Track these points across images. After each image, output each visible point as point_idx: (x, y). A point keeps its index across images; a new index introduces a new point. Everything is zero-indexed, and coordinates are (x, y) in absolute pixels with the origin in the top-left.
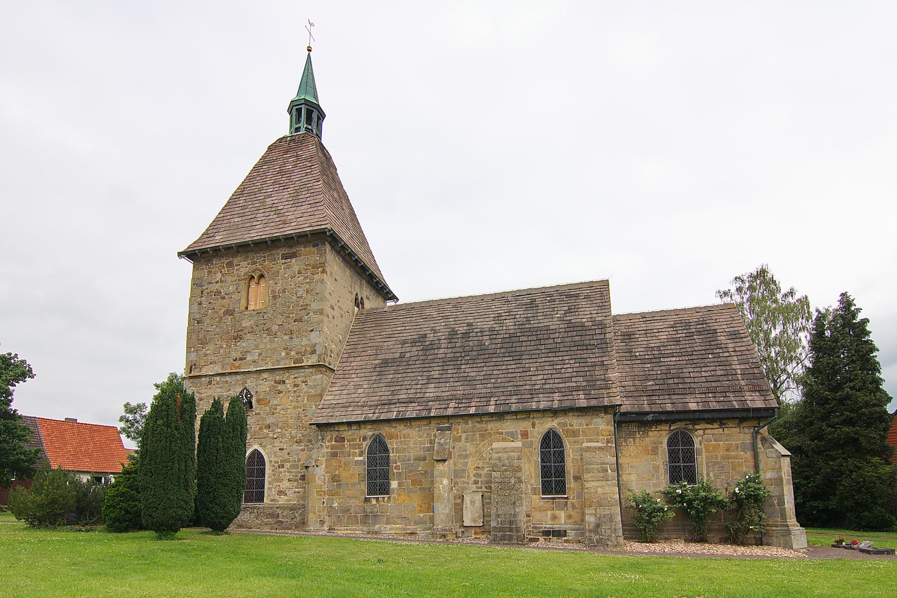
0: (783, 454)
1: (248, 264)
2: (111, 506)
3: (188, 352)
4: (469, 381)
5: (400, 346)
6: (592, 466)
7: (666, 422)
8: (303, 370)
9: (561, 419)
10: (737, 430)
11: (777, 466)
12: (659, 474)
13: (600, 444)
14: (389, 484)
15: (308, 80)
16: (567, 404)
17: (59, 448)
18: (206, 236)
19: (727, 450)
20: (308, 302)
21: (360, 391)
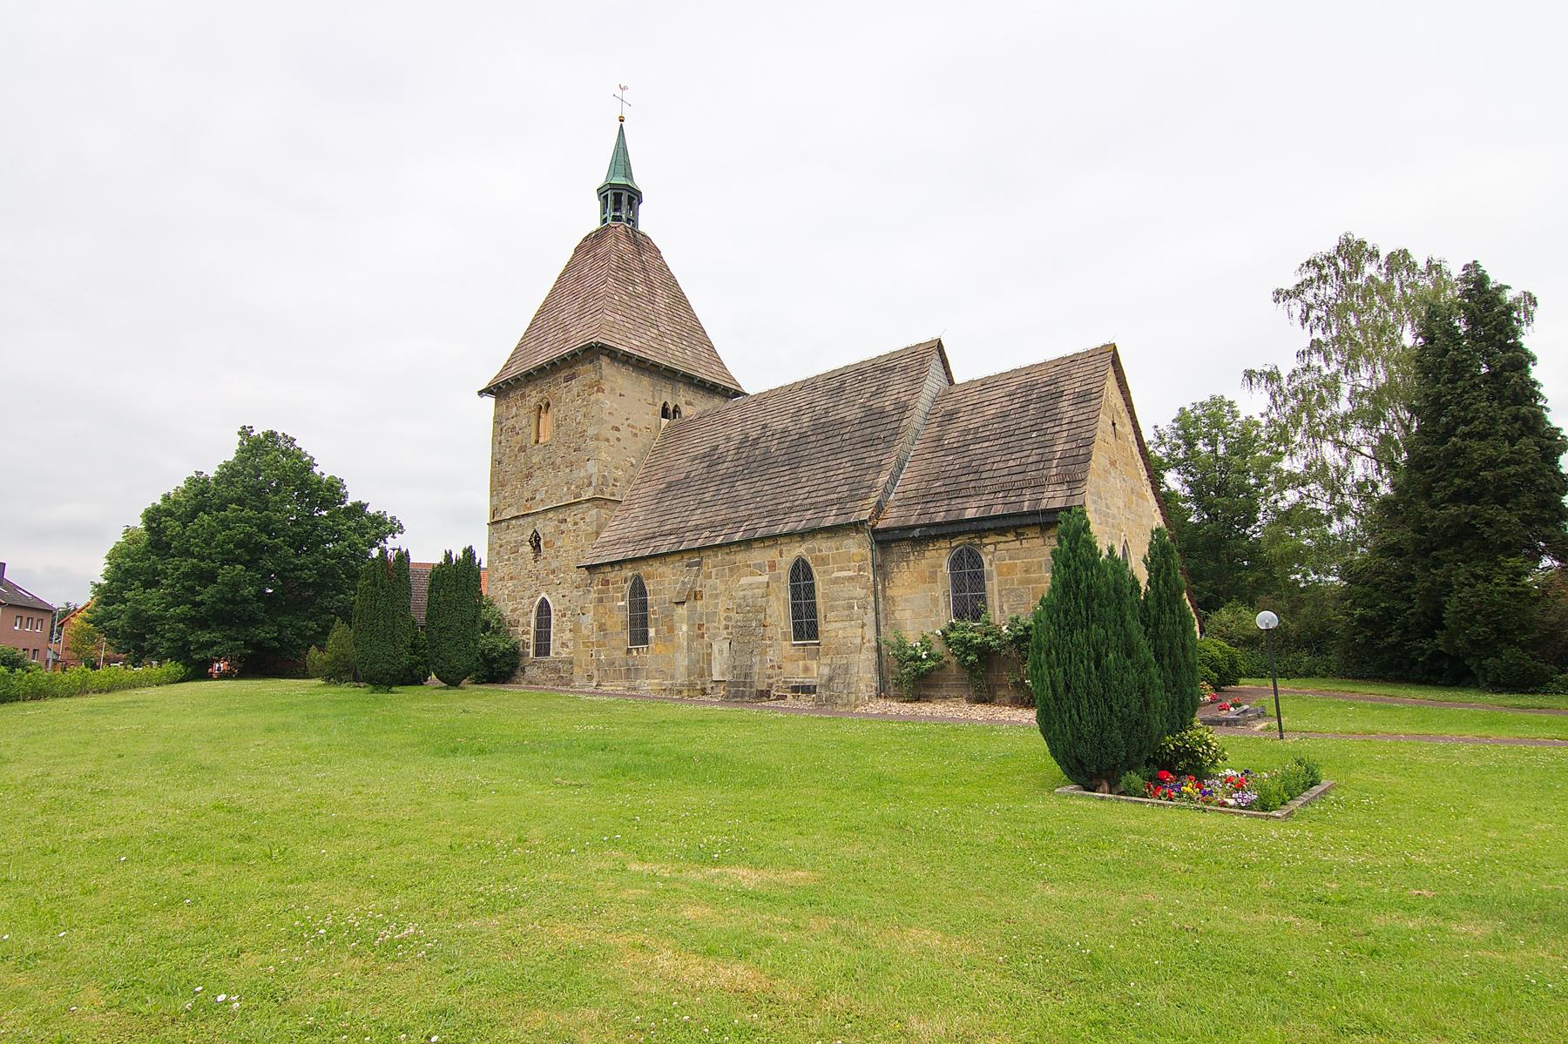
7: (944, 536)
8: (580, 506)
9: (808, 544)
10: (1040, 541)
13: (851, 573)
14: (646, 633)
16: (812, 524)
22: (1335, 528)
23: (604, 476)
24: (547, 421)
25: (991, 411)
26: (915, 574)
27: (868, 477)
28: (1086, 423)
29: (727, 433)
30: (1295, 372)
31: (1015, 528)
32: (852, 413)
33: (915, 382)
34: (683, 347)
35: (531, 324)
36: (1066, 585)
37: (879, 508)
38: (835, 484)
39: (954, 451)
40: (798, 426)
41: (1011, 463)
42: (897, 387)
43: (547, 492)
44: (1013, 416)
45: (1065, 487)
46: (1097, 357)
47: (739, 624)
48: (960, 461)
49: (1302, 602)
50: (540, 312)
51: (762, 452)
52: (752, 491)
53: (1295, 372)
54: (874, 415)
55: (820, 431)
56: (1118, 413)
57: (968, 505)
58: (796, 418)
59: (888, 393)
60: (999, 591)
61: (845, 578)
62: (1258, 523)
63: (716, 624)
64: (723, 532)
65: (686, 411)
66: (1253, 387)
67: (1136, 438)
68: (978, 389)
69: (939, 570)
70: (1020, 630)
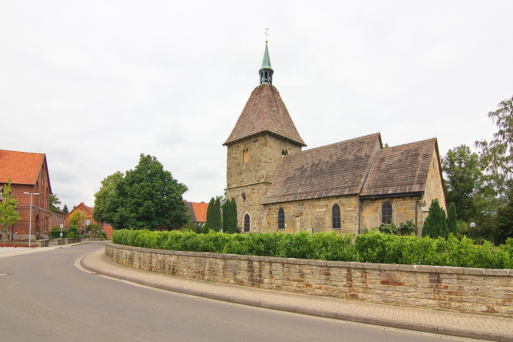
0: (423, 211)
1: (243, 146)
2: (204, 232)
3: (227, 180)
4: (313, 185)
5: (294, 171)
6: (348, 218)
7: (381, 199)
8: (260, 184)
9: (339, 200)
10: (410, 201)
11: (421, 216)
12: (378, 220)
13: (352, 209)
14: (284, 225)
15: (267, 59)
16: (341, 194)
17: (199, 214)
18: (231, 136)
19: (405, 210)
20: (261, 159)
21: (278, 191)
22: (498, 196)
23: (267, 175)
24: (247, 156)
25: (396, 159)
26: (371, 210)
27: (357, 179)
28: (426, 165)
29: (307, 161)
30: (492, 141)
31: (403, 197)
32: (351, 157)
33: (372, 148)
34: (288, 129)
35: (238, 121)
36: (432, 215)
37: (362, 189)
38: (347, 181)
39: (384, 172)
40: (332, 160)
41: (403, 177)
42: (365, 149)
43: (248, 179)
44: (403, 161)
45: (419, 185)
46: (431, 142)
47: (316, 223)
48: (386, 175)
49: (483, 221)
50: (241, 116)
51: (320, 169)
52: (318, 182)
53: (492, 141)
54: (358, 159)
55: (340, 163)
56: (435, 160)
57: (389, 189)
58: (331, 158)
59: (363, 151)
60: (396, 215)
61: (350, 210)
62: (473, 192)
63: (307, 223)
64: (311, 195)
65: (289, 152)
66: (477, 147)
67: (439, 168)
68: (391, 151)
69: (378, 208)
70: (403, 226)
